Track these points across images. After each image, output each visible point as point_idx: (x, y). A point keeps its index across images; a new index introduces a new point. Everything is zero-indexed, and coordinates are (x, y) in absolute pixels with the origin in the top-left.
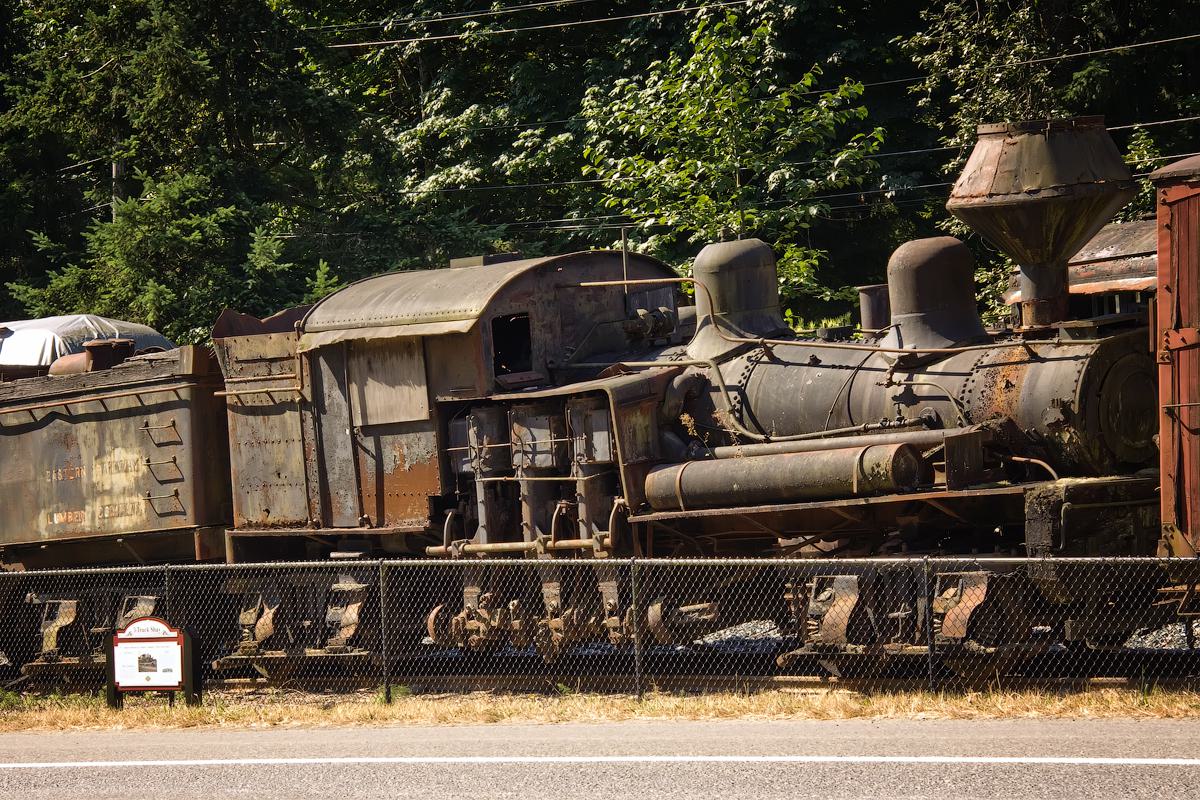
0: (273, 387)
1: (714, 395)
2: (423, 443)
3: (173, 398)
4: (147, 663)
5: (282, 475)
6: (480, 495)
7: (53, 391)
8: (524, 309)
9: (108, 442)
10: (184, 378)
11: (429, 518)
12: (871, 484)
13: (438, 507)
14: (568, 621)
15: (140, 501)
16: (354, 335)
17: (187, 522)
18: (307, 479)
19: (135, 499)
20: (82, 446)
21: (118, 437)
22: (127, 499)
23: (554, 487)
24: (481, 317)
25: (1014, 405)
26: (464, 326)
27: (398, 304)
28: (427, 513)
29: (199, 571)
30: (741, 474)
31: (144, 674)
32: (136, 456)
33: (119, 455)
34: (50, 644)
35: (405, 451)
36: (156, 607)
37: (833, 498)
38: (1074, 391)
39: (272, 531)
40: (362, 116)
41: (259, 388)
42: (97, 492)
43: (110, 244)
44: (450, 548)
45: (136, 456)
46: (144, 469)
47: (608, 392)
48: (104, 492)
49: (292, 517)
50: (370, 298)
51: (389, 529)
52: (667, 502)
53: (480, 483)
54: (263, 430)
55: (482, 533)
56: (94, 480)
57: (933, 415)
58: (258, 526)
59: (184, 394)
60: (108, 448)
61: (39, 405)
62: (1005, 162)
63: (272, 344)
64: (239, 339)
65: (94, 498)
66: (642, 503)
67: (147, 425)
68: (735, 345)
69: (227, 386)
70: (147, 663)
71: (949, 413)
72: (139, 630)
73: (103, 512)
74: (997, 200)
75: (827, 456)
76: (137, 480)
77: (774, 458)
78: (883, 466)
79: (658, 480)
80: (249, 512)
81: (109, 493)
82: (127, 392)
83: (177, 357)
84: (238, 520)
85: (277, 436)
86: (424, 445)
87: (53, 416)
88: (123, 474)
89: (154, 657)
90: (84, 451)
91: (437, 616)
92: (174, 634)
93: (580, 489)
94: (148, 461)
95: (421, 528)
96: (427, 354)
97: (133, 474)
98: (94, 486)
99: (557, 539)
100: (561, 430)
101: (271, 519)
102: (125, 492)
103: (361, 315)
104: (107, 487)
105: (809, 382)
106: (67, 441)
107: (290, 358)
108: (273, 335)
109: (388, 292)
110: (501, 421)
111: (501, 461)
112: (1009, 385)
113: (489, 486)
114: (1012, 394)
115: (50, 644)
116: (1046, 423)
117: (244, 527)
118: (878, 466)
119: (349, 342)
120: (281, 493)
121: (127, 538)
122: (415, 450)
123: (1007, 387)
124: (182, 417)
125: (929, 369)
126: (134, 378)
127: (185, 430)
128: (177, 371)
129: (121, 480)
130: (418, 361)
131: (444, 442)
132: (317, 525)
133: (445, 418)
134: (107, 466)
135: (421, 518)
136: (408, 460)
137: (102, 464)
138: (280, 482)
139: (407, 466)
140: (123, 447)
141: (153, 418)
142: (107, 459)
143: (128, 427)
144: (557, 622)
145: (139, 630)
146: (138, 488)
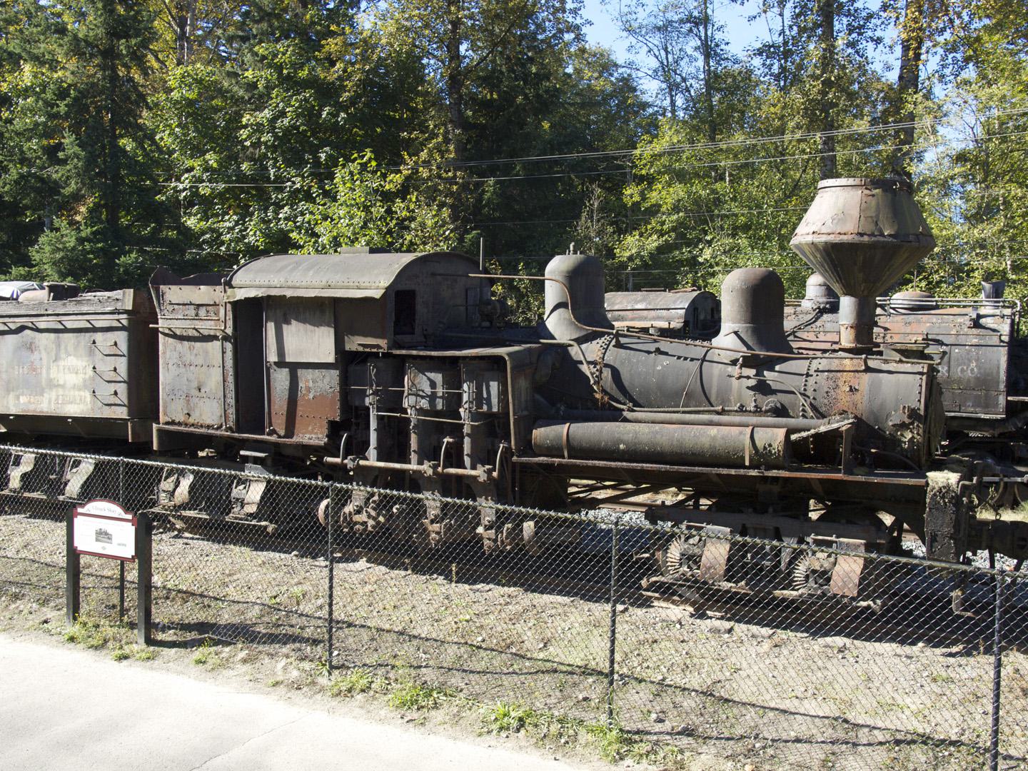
0: (199, 325)
1: (580, 366)
2: (327, 380)
3: (116, 324)
4: (102, 535)
5: (203, 390)
6: (373, 424)
7: (23, 312)
8: (413, 287)
9: (63, 351)
10: (126, 312)
11: (327, 436)
12: (762, 458)
13: (335, 429)
14: (449, 527)
15: (87, 395)
16: (274, 292)
17: (122, 413)
18: (225, 396)
19: (82, 393)
20: (43, 352)
21: (71, 349)
22: (77, 393)
23: (440, 425)
24: (387, 289)
25: (859, 406)
26: (377, 294)
27: (311, 273)
28: (326, 432)
29: (152, 467)
30: (629, 437)
31: (100, 544)
32: (84, 364)
33: (72, 361)
34: (15, 483)
35: (311, 384)
36: (95, 469)
37: (719, 466)
38: (919, 401)
39: (192, 429)
40: (302, 124)
41: (187, 324)
42: (52, 385)
43: (44, 250)
44: (346, 461)
45: (84, 364)
46: (90, 372)
47: (507, 358)
48: (59, 386)
49: (209, 422)
50: (286, 266)
51: (295, 439)
52: (554, 450)
53: (373, 415)
54: (188, 356)
55: (372, 452)
56: (52, 376)
57: (779, 405)
58: (179, 424)
59: (125, 322)
60: (63, 356)
61: (12, 320)
62: (867, 208)
63: (203, 293)
64: (173, 287)
65: (51, 389)
66: (527, 446)
67: (94, 342)
68: (583, 333)
69: (160, 321)
70: (102, 535)
71: (794, 405)
72: (97, 509)
73: (57, 399)
74: (866, 238)
75: (713, 431)
76: (85, 381)
77: (657, 427)
78: (775, 445)
79: (541, 434)
80: (171, 410)
81: (63, 386)
82: (80, 317)
83: (120, 297)
84: (162, 418)
85: (200, 361)
86: (328, 382)
87: (22, 329)
88: (74, 375)
89: (109, 532)
90: (44, 355)
91: (327, 507)
92: (129, 517)
93: (466, 430)
94: (94, 368)
95: (322, 443)
96: (336, 312)
97: (81, 376)
98: (51, 380)
99: (445, 467)
100: (454, 382)
101: (191, 420)
102: (74, 387)
103: (276, 280)
104: (61, 382)
105: (659, 368)
106: (30, 347)
107: (215, 305)
108: (202, 287)
109: (298, 264)
110: (396, 368)
111: (392, 402)
112: (852, 390)
113: (380, 419)
114: (857, 396)
115: (15, 483)
116: (891, 424)
117: (167, 423)
118: (770, 445)
119: (269, 297)
120: (201, 403)
121: (75, 419)
122: (320, 384)
123: (851, 390)
124: (122, 338)
125: (777, 368)
126: (85, 309)
127: (124, 347)
128: (119, 306)
129: (72, 379)
130: (329, 315)
131: (345, 381)
132: (230, 429)
133: (347, 362)
134: (61, 368)
135: (320, 436)
136: (313, 392)
137: (58, 366)
138: (200, 395)
139: (311, 396)
140: (75, 356)
141: (99, 337)
142: (62, 363)
143: (79, 342)
144: (436, 527)
145: (97, 509)
146: (85, 387)
